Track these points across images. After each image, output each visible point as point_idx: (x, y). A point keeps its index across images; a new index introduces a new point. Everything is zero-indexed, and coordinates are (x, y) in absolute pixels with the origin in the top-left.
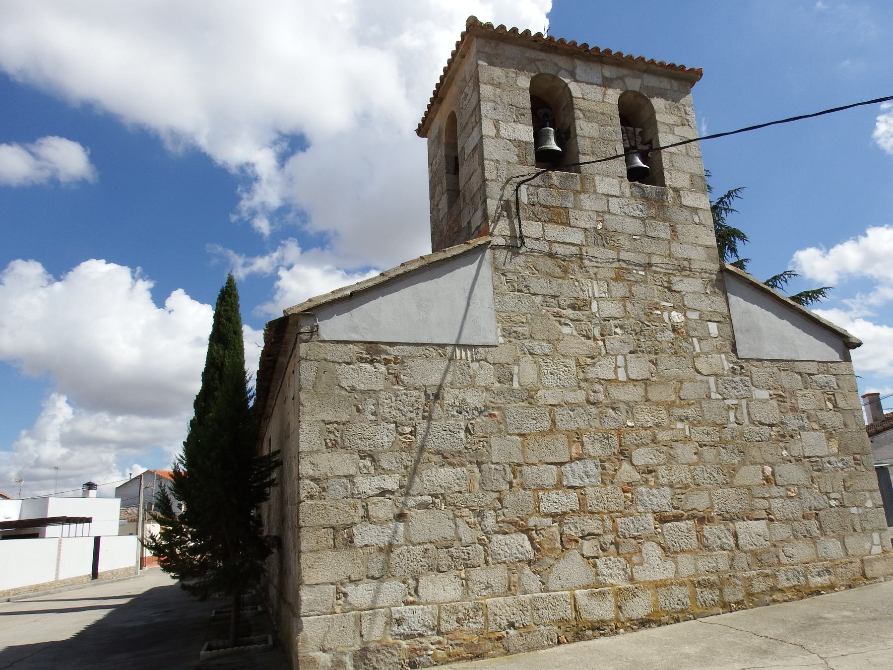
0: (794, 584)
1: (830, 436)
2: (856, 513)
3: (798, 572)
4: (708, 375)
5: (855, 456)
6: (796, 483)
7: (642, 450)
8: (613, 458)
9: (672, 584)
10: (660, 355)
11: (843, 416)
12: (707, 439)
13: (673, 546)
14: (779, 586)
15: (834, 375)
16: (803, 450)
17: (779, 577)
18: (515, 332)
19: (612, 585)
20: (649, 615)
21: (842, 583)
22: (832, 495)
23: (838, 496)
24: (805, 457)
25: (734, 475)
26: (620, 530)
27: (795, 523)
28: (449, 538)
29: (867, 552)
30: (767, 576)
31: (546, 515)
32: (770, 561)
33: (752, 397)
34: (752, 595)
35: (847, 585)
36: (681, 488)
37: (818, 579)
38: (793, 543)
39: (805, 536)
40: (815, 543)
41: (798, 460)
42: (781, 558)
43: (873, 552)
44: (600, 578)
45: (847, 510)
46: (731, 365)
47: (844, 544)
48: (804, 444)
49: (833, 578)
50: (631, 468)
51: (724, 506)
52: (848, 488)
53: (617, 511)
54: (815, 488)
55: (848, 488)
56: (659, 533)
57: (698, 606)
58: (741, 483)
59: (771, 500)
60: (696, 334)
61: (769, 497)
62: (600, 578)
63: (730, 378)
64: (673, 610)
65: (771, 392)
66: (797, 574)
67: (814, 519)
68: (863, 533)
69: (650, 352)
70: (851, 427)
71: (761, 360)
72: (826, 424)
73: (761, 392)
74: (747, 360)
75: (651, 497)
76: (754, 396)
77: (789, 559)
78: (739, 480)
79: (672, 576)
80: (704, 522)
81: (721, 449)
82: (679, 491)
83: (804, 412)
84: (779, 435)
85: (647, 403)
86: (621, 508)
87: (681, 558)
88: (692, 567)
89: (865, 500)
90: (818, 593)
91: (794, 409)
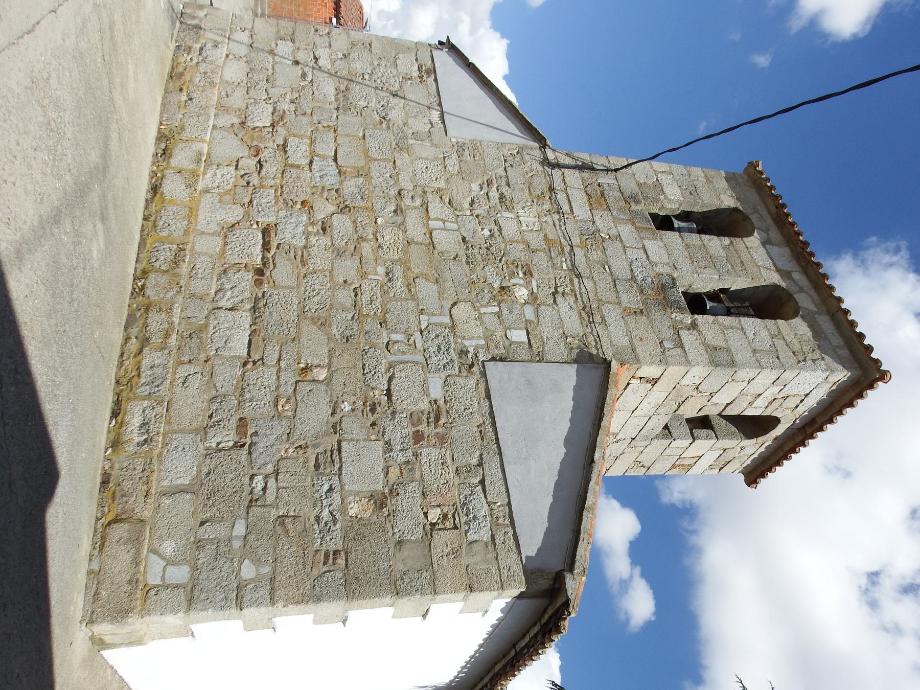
0: (143, 375)
1: (380, 502)
2: (234, 533)
3: (158, 386)
4: (451, 316)
5: (343, 554)
6: (299, 415)
7: (349, 225)
8: (341, 199)
9: (190, 222)
10: (467, 267)
11: (416, 541)
12: (364, 299)
13: (234, 235)
14: (146, 350)
15: (493, 538)
16: (352, 440)
17: (160, 353)
18: (464, 150)
19: (205, 174)
20: (162, 193)
21: (117, 466)
22: (272, 483)
23: (270, 497)
24: (339, 442)
25: (315, 323)
26: (262, 190)
27: (236, 402)
28: (275, 82)
29: (156, 544)
30: (167, 335)
31: (286, 141)
32: (186, 350)
33: (430, 372)
34: (147, 311)
35: (110, 475)
36: (302, 256)
37: (136, 421)
38: (205, 391)
39: (211, 417)
40: (196, 431)
41: (335, 428)
42: (187, 366)
43: (154, 558)
44: (214, 167)
45: (243, 512)
46: (471, 350)
47: (182, 490)
48: (362, 443)
49: (130, 448)
50: (329, 212)
51: (275, 302)
52: (283, 524)
53: (282, 192)
54: (286, 451)
55: (283, 524)
56: (251, 225)
57: (155, 243)
58: (305, 330)
59: (275, 370)
60: (505, 311)
61: (280, 368)
62: (214, 167)
63: (453, 346)
64: (159, 217)
65: (441, 402)
66: (156, 384)
67: (237, 439)
68: (194, 542)
69: (468, 257)
70: (398, 556)
71: (488, 396)
72: (399, 498)
73: (439, 386)
74: (484, 374)
75: (294, 225)
76: (430, 375)
77: (181, 380)
78: (308, 328)
79: (199, 228)
80: (256, 274)
81: (352, 314)
82: (300, 253)
83: (416, 455)
84: (374, 404)
85: (405, 242)
86: (285, 195)
87: (218, 242)
88: (204, 249)
89: (257, 562)
90: (115, 414)
91: (418, 437)
